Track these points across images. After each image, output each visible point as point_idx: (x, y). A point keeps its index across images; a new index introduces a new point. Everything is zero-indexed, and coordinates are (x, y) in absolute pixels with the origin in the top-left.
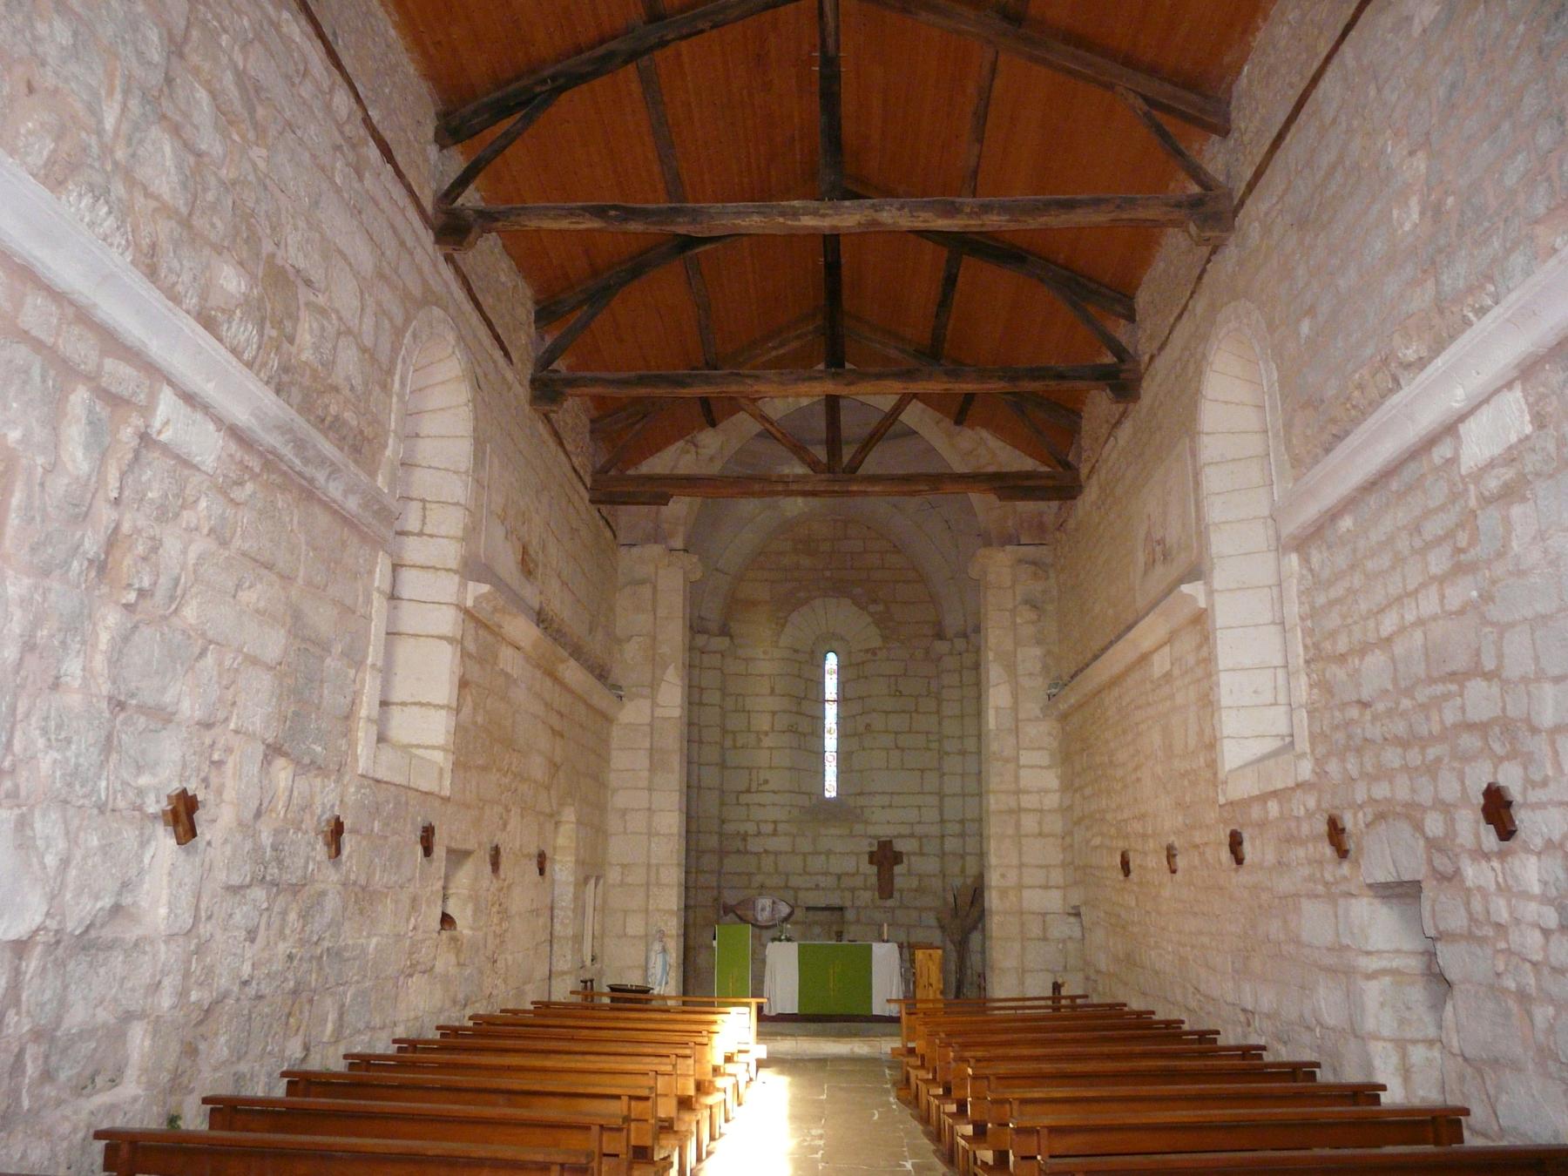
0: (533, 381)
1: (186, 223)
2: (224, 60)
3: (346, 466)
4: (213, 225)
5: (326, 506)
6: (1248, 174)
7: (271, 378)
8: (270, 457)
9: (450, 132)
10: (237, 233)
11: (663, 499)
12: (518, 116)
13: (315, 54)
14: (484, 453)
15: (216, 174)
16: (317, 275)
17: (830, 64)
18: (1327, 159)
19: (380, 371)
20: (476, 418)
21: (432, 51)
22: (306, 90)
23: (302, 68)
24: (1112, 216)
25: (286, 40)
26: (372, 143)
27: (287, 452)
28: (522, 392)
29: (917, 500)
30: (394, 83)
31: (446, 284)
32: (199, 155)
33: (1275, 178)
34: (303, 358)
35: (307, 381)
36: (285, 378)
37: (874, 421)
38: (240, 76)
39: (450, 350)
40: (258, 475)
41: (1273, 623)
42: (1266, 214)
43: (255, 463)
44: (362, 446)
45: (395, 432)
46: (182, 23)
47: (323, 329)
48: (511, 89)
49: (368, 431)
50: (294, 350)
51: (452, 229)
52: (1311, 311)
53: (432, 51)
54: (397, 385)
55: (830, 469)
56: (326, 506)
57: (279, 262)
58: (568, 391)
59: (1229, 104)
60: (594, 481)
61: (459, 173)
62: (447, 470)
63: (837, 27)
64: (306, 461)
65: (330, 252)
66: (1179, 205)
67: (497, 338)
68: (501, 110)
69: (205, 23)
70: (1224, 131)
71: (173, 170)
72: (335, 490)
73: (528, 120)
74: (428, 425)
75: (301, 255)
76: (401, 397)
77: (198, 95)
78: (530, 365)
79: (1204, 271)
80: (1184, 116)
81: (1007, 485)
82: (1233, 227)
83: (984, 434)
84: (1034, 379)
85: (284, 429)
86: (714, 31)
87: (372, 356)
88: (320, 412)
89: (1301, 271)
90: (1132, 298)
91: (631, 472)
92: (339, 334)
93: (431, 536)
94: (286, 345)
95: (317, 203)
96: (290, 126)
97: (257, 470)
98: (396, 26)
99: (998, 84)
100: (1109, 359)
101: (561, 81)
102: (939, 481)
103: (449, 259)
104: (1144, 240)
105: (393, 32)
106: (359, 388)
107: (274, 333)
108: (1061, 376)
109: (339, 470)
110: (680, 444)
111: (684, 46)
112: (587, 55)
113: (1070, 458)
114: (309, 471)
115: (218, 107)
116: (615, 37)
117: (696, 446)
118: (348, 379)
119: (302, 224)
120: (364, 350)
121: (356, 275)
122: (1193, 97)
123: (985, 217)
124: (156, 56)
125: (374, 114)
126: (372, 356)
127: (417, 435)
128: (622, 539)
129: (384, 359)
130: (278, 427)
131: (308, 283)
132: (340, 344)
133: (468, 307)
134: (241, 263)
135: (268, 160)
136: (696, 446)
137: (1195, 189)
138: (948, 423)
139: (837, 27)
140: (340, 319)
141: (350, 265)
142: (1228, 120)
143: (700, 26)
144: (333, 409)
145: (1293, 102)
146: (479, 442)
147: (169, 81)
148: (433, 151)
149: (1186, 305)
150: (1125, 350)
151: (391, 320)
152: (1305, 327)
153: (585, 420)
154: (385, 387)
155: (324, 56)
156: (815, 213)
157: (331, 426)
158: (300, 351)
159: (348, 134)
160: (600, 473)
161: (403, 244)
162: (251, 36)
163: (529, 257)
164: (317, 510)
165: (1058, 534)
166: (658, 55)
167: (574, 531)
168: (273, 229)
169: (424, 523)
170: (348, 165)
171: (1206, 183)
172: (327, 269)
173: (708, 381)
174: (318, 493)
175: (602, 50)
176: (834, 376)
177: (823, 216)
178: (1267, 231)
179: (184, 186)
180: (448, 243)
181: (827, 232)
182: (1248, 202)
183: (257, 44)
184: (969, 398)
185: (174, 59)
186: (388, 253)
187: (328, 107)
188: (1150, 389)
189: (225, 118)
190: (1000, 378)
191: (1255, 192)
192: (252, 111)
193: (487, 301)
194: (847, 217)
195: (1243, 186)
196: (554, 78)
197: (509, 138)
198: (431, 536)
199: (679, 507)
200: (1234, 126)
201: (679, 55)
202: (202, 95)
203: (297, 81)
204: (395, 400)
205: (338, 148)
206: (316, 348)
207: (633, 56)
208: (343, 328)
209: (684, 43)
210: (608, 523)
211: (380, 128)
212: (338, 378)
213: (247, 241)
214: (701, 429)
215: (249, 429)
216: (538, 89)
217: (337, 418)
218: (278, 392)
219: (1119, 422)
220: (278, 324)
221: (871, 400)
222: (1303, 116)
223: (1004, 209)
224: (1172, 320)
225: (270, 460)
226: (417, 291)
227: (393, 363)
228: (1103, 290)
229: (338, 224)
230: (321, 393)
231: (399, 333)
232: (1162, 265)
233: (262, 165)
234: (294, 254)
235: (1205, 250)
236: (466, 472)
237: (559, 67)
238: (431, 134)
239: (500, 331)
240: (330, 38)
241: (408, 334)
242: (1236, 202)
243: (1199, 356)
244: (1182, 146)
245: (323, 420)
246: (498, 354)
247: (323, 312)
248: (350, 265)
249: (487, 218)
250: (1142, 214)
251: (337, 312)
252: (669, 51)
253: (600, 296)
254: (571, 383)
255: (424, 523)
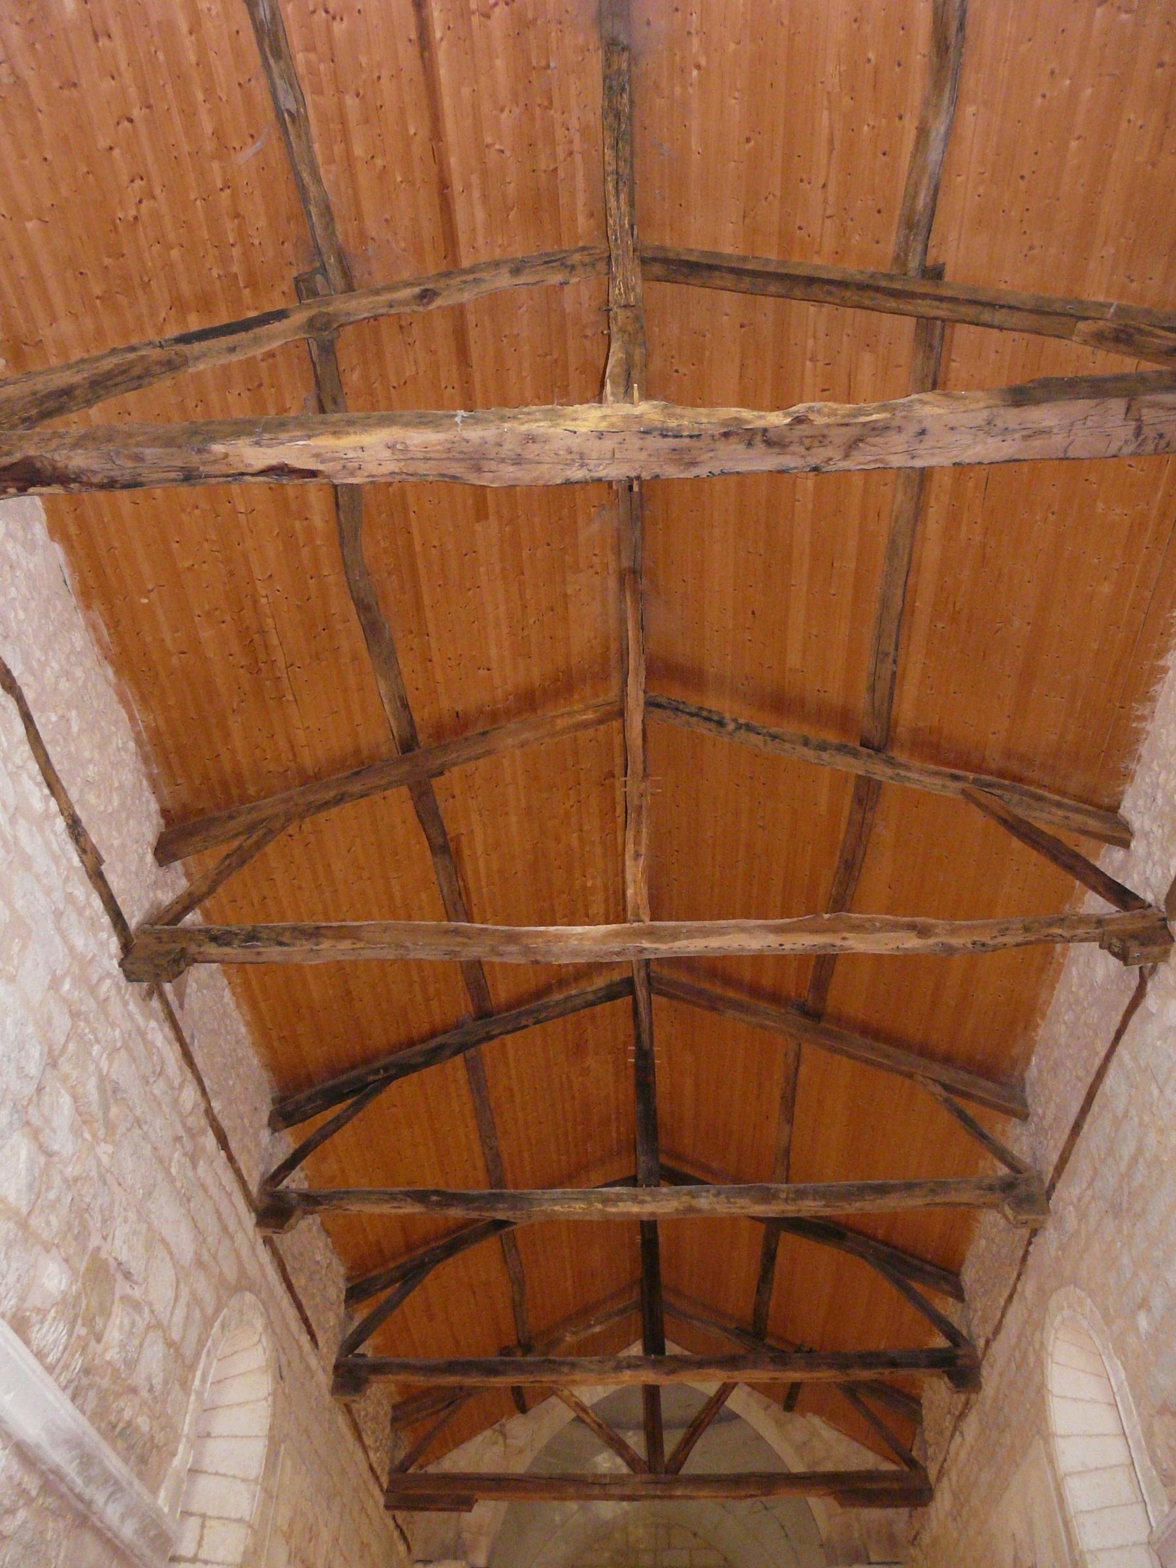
0: (336, 1367)
1: (24, 1225)
2: (92, 1067)
3: (131, 1484)
4: (48, 1223)
5: (98, 1533)
6: (1055, 1158)
7: (70, 1381)
8: (51, 1477)
9: (284, 1116)
10: (70, 1228)
11: (467, 1504)
12: (349, 1102)
13: (172, 1055)
14: (277, 1454)
15: (61, 1172)
16: (136, 1267)
17: (644, 1057)
18: (1127, 1150)
19: (183, 1365)
20: (274, 1415)
21: (276, 1044)
22: (159, 1088)
23: (158, 1070)
24: (928, 1200)
25: (149, 1045)
26: (210, 1132)
27: (71, 1470)
28: (324, 1379)
29: (749, 1501)
30: (239, 1075)
31: (261, 1266)
32: (50, 1155)
33: (1080, 1163)
34: (108, 1358)
35: (106, 1383)
36: (85, 1381)
37: (699, 1406)
38: (102, 1079)
39: (256, 1338)
40: (33, 1500)
41: (1137, 1502)
42: (1079, 1199)
43: (32, 1484)
44: (146, 1455)
45: (188, 1438)
46: (63, 1039)
47: (133, 1324)
48: (344, 1077)
49: (160, 1438)
50: (99, 1348)
51: (274, 1211)
52: (1144, 1304)
53: (276, 1044)
54: (197, 1383)
55: (651, 1469)
56: (98, 1533)
57: (103, 1255)
58: (372, 1377)
59: (1023, 1090)
60: (392, 1482)
61: (288, 1156)
62: (234, 1477)
63: (651, 1024)
64: (89, 1480)
65: (155, 1241)
66: (991, 1188)
67: (305, 1320)
68: (333, 1096)
69: (81, 1037)
70: (1024, 1116)
71: (24, 1172)
72: (112, 1513)
73: (357, 1107)
74: (221, 1424)
75: (125, 1248)
76: (200, 1395)
77: (61, 1101)
78: (335, 1349)
79: (1026, 1253)
80: (983, 1102)
81: (849, 1488)
82: (1049, 1211)
83: (816, 1421)
84: (869, 1365)
85: (75, 1444)
86: (537, 1026)
87: (177, 1350)
88: (113, 1418)
89: (1125, 1260)
90: (957, 1275)
91: (432, 1469)
92: (148, 1328)
93: (206, 1562)
94: (93, 1342)
95: (150, 1193)
96: (139, 1122)
97: (34, 1493)
98: (247, 1024)
99: (804, 1070)
100: (940, 1342)
101: (392, 1072)
102: (771, 1482)
103: (267, 1241)
104: (962, 1220)
105: (243, 1030)
106: (158, 1388)
107: (83, 1331)
108: (893, 1364)
109: (122, 1489)
110: (488, 1433)
111: (508, 1038)
112: (418, 1047)
113: (914, 1453)
114: (88, 1492)
115: (77, 1109)
116: (445, 1032)
117: (505, 1436)
118: (149, 1378)
119: (132, 1216)
120: (170, 1344)
121: (175, 1263)
122: (989, 1084)
123: (800, 1202)
124: (33, 1069)
125: (216, 1105)
126: (177, 1350)
127: (209, 1435)
128: (418, 1552)
129: (188, 1352)
130: (67, 1442)
131: (127, 1275)
132: (148, 1340)
133: (280, 1289)
134: (66, 1260)
135: (112, 1156)
136: (505, 1436)
137: (1003, 1170)
138: (776, 1408)
139: (651, 1024)
140: (152, 1312)
141: (171, 1253)
142: (1025, 1105)
143: (524, 1023)
144: (127, 1414)
145: (1084, 1093)
146: (275, 1441)
147: (40, 1090)
148: (265, 1135)
149: (1014, 1289)
150: (960, 1334)
151: (202, 1310)
152: (1143, 1321)
153: (387, 1408)
154: (185, 1385)
155: (180, 1057)
156: (635, 1199)
157: (119, 1433)
158: (106, 1350)
159: (189, 1124)
160: (399, 1470)
161: (225, 1229)
162: (119, 1044)
163: (275, 1009)
164: (88, 1538)
165: (912, 1551)
166: (484, 1047)
167: (364, 1546)
168: (104, 1221)
169: (200, 1545)
170: (185, 1154)
171: (1014, 1166)
172: (148, 1260)
173: (520, 1368)
174: (94, 1519)
175: (433, 1043)
176: (655, 1365)
177: (643, 1202)
178: (1083, 1216)
179: (30, 1186)
180: (268, 1226)
181: (645, 1218)
182: (1059, 1186)
183: (123, 1051)
184: (795, 1387)
185: (48, 1068)
186: (210, 1239)
187: (175, 1102)
188: (991, 1377)
189: (82, 1117)
190: (831, 1366)
191: (1064, 1176)
192: (106, 1109)
193: (299, 1282)
194: (662, 1203)
195: (1051, 1169)
196: (386, 1068)
197: (337, 1124)
198: (206, 1562)
199: (486, 1513)
200: (1031, 1110)
201: (504, 1045)
202: (66, 1100)
203: (152, 1080)
204: (193, 1398)
205: (178, 1139)
206: (123, 1345)
207: (461, 1048)
208: (153, 1322)
209: (509, 1037)
210: (402, 1532)
211: (219, 1117)
212: (138, 1379)
213: (76, 1237)
214: (511, 1415)
215: (38, 1446)
216: (371, 1078)
217: (129, 1424)
218: (73, 1399)
219: (962, 1416)
220: (89, 1322)
221: (697, 1385)
222: (1095, 1108)
223: (817, 1194)
224: (1002, 1302)
225: (51, 1481)
226: (231, 1276)
227: (197, 1355)
228: (928, 1268)
229: (167, 1214)
230: (118, 1395)
231: (208, 1323)
232: (983, 1243)
233: (105, 1160)
234: (121, 1246)
235: (1025, 1232)
236: (256, 1481)
237: (392, 1058)
238: (265, 1120)
239: (309, 1313)
240: (188, 1040)
241: (217, 1324)
242: (1047, 1184)
243: (1037, 1346)
244: (986, 1131)
245: (114, 1427)
246: (305, 1339)
247: (137, 1306)
248: (171, 1253)
249: (311, 1201)
250: (954, 1197)
251: (151, 1304)
252: (495, 1043)
253: (412, 1275)
254: (378, 1369)
255: (200, 1545)
